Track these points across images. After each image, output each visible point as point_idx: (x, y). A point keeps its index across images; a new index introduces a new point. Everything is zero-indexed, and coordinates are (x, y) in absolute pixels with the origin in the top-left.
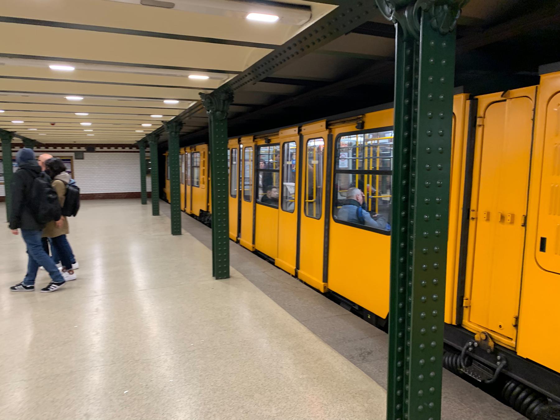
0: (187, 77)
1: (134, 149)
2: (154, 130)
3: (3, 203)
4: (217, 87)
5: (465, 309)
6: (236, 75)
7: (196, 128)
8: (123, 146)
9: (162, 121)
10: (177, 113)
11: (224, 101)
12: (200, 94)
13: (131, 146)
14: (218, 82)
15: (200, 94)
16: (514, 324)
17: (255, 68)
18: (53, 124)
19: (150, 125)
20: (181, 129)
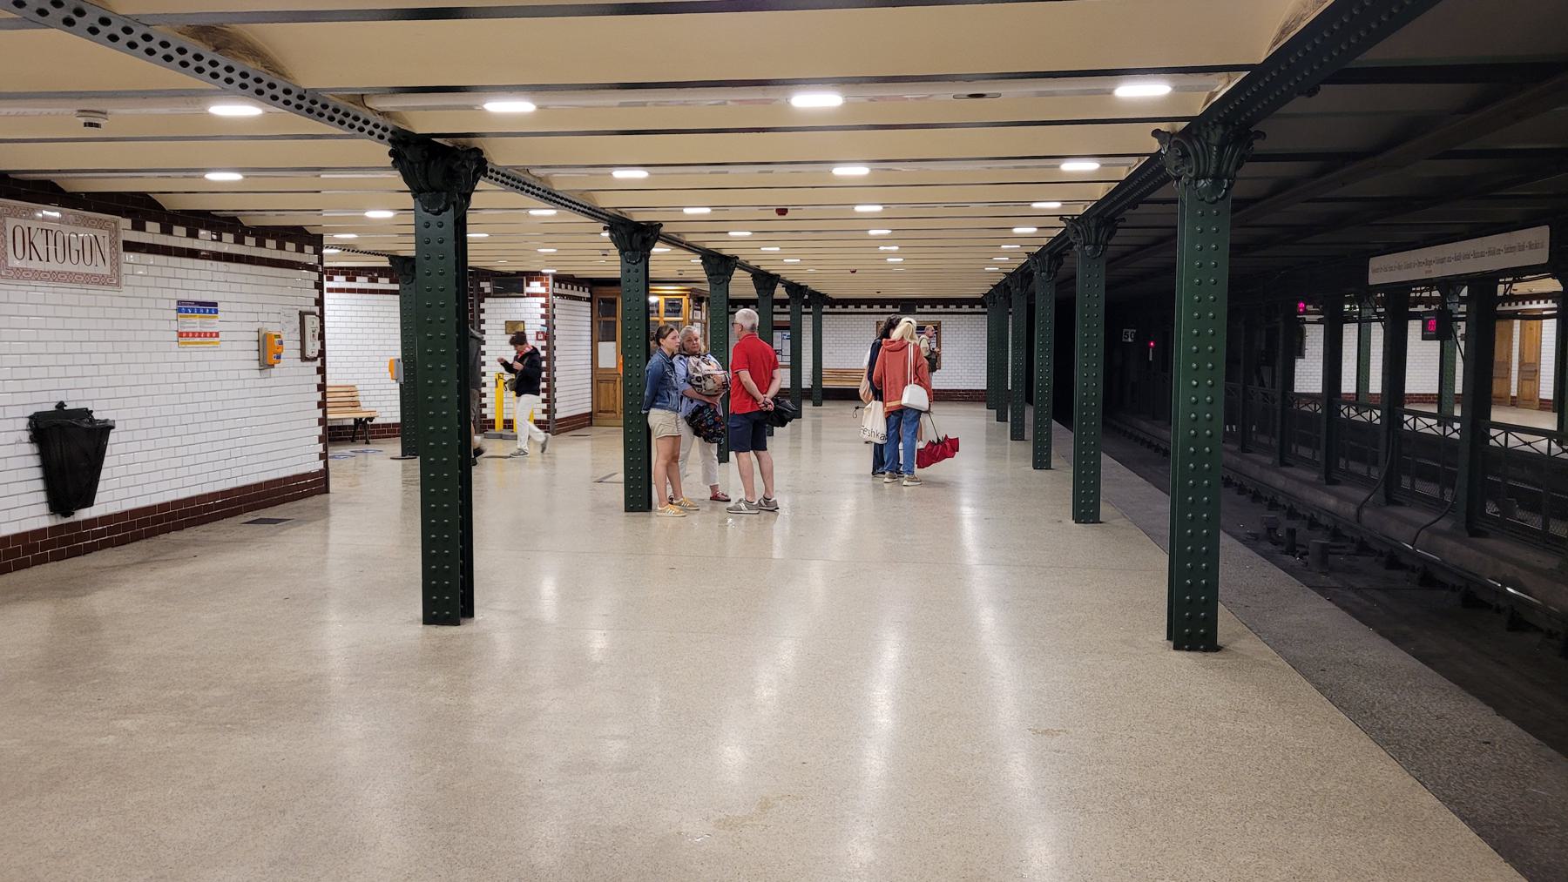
0: (1110, 92)
1: (978, 308)
2: (1045, 242)
3: (335, 424)
4: (1199, 110)
5: (386, 407)
6: (1245, 74)
7: (1126, 249)
8: (959, 302)
9: (1062, 218)
10: (1100, 191)
11: (1221, 148)
12: (1156, 133)
13: (972, 302)
14: (1200, 97)
15: (1156, 133)
16: (710, 495)
17: (1214, 109)
18: (782, 212)
19: (1033, 230)
20: (1111, 235)
